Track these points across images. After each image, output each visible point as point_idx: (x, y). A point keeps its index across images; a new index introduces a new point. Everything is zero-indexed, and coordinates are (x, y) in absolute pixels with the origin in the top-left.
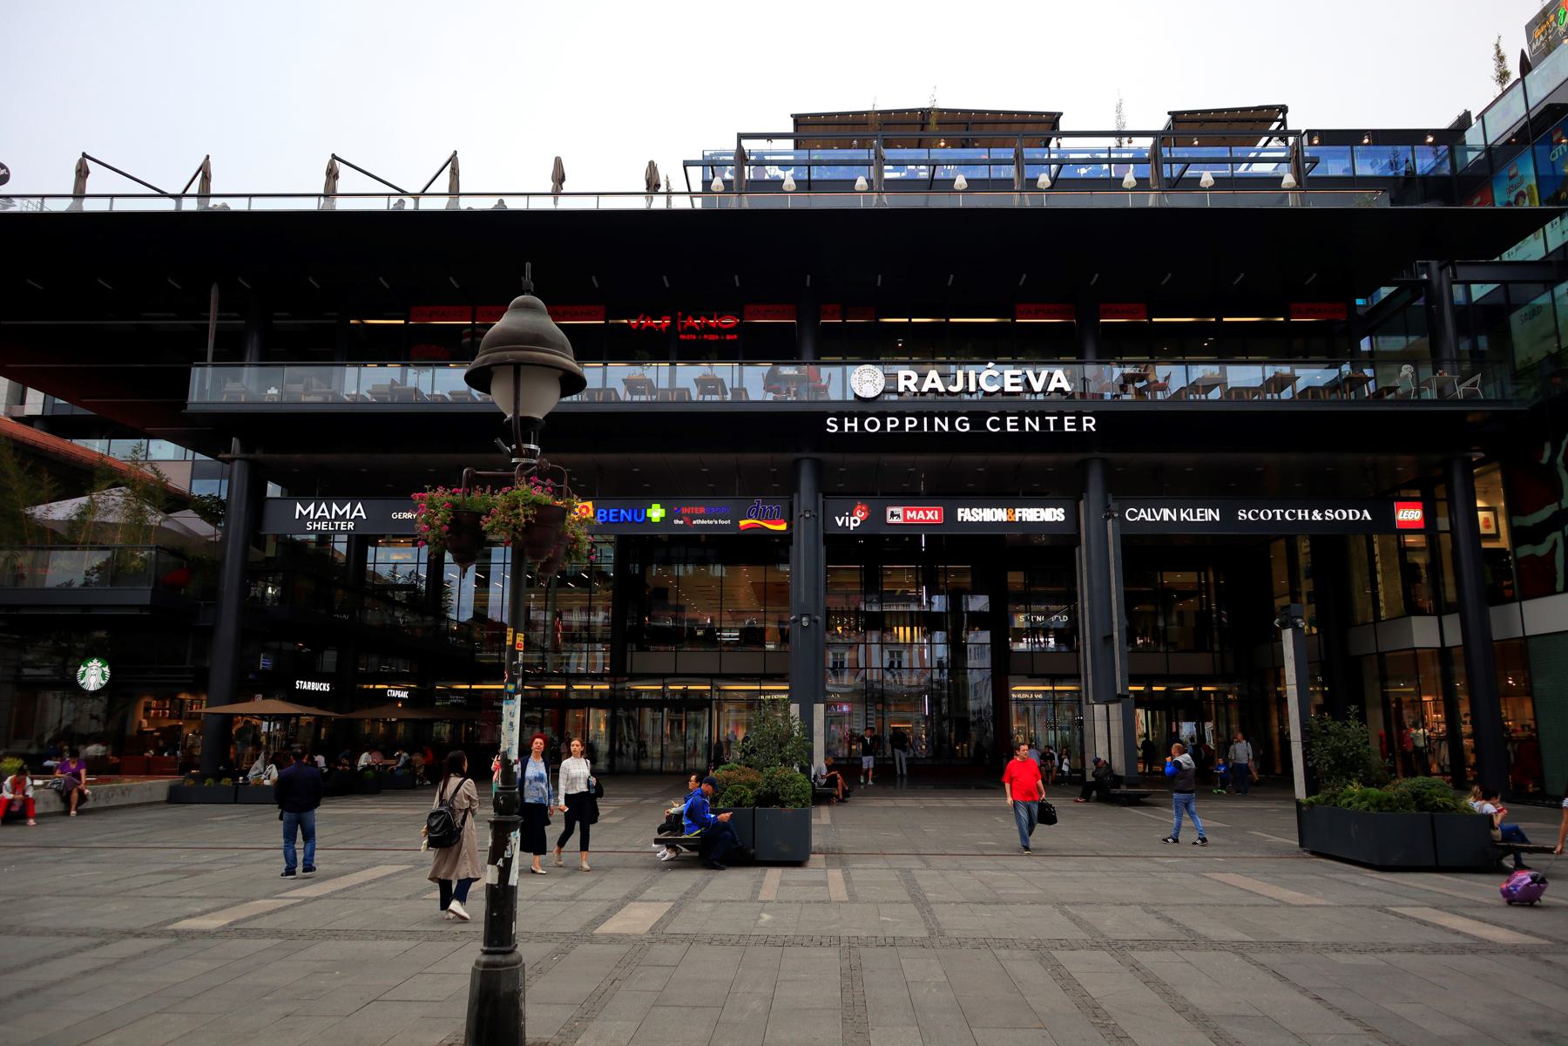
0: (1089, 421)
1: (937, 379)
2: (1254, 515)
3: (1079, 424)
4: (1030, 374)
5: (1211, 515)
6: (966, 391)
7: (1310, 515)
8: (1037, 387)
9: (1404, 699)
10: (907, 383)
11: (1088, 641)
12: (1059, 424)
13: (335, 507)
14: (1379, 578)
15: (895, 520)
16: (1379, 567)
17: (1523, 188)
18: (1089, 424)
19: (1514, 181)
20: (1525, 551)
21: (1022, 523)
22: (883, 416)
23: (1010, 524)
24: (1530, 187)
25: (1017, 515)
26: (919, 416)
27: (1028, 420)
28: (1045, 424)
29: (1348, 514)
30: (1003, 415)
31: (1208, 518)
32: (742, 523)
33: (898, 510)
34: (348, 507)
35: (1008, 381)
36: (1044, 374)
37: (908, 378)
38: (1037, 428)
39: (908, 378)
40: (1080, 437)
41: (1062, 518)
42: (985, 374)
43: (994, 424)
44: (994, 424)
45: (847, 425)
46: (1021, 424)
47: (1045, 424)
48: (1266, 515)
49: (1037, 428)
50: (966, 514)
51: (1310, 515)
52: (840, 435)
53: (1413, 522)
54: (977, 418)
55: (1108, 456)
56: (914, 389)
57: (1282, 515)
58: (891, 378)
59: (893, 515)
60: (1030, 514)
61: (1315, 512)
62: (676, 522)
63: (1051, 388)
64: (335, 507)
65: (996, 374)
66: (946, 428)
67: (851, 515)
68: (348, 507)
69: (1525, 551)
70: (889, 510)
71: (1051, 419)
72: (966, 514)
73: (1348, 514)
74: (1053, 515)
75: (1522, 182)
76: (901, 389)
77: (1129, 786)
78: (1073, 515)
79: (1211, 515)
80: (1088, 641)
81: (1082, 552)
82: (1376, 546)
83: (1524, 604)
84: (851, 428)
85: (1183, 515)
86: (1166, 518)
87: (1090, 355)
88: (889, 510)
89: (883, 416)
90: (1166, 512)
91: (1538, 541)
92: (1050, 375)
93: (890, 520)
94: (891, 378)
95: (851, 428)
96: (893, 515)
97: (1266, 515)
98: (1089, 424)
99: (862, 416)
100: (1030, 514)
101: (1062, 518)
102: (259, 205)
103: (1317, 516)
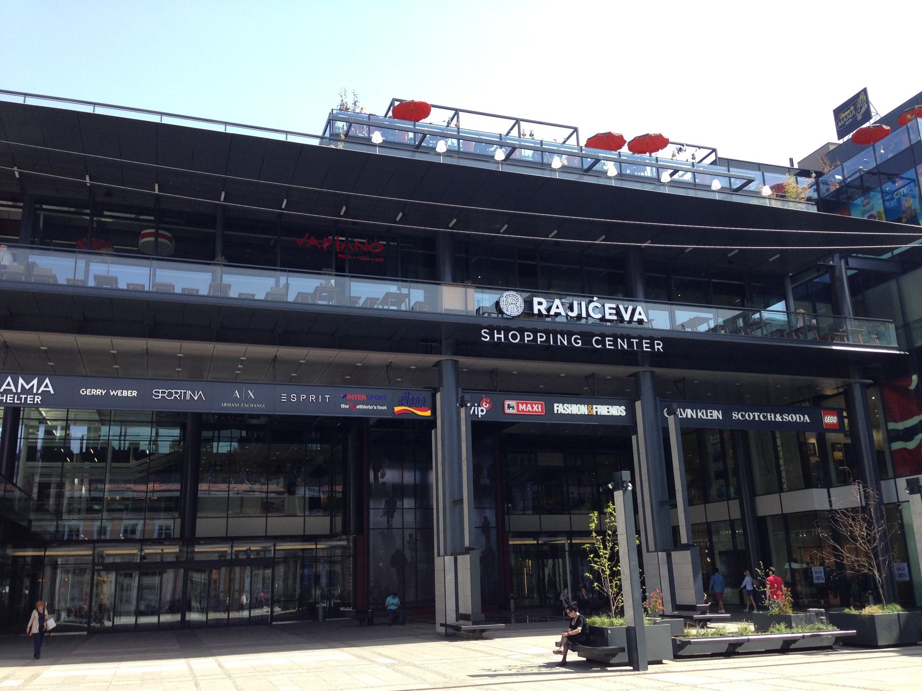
0: (659, 344)
1: (560, 306)
2: (743, 416)
3: (652, 346)
4: (621, 307)
5: (716, 415)
6: (579, 317)
7: (775, 417)
8: (627, 317)
9: (60, 561)
10: (540, 307)
11: (441, 505)
12: (640, 345)
13: (21, 381)
14: (781, 462)
15: (511, 411)
16: (781, 454)
17: (874, 213)
18: (659, 347)
19: (867, 208)
20: (897, 445)
21: (597, 416)
22: (522, 331)
23: (589, 416)
24: (879, 213)
25: (595, 410)
26: (547, 332)
27: (619, 340)
28: (630, 344)
29: (796, 418)
30: (603, 336)
31: (715, 417)
32: (397, 409)
33: (513, 403)
34: (35, 382)
35: (607, 311)
36: (630, 309)
37: (540, 303)
38: (626, 347)
39: (540, 303)
40: (654, 355)
41: (624, 414)
42: (592, 305)
43: (597, 342)
44: (597, 342)
45: (496, 336)
46: (615, 343)
47: (630, 344)
48: (749, 416)
49: (626, 347)
50: (560, 408)
51: (775, 417)
52: (491, 343)
53: (833, 424)
54: (586, 336)
55: (657, 370)
56: (544, 312)
57: (759, 416)
58: (529, 304)
59: (509, 407)
60: (602, 410)
61: (778, 415)
62: (343, 406)
63: (635, 319)
64: (21, 381)
65: (599, 306)
66: (566, 343)
67: (479, 406)
68: (35, 382)
69: (897, 445)
70: (507, 402)
71: (635, 341)
72: (560, 408)
73: (796, 418)
74: (618, 411)
75: (872, 209)
76: (536, 311)
77: (474, 623)
78: (631, 411)
79: (716, 415)
80: (441, 505)
81: (437, 435)
82: (778, 441)
83: (897, 480)
84: (499, 339)
85: (700, 414)
86: (689, 416)
87: (641, 295)
88: (507, 402)
89: (522, 331)
90: (689, 411)
91: (910, 438)
92: (634, 311)
93: (507, 411)
94: (529, 304)
95: (499, 339)
96: (509, 407)
97: (749, 416)
98: (659, 347)
99: (507, 330)
100: (602, 410)
101: (624, 414)
102: (292, 139)
103: (779, 418)
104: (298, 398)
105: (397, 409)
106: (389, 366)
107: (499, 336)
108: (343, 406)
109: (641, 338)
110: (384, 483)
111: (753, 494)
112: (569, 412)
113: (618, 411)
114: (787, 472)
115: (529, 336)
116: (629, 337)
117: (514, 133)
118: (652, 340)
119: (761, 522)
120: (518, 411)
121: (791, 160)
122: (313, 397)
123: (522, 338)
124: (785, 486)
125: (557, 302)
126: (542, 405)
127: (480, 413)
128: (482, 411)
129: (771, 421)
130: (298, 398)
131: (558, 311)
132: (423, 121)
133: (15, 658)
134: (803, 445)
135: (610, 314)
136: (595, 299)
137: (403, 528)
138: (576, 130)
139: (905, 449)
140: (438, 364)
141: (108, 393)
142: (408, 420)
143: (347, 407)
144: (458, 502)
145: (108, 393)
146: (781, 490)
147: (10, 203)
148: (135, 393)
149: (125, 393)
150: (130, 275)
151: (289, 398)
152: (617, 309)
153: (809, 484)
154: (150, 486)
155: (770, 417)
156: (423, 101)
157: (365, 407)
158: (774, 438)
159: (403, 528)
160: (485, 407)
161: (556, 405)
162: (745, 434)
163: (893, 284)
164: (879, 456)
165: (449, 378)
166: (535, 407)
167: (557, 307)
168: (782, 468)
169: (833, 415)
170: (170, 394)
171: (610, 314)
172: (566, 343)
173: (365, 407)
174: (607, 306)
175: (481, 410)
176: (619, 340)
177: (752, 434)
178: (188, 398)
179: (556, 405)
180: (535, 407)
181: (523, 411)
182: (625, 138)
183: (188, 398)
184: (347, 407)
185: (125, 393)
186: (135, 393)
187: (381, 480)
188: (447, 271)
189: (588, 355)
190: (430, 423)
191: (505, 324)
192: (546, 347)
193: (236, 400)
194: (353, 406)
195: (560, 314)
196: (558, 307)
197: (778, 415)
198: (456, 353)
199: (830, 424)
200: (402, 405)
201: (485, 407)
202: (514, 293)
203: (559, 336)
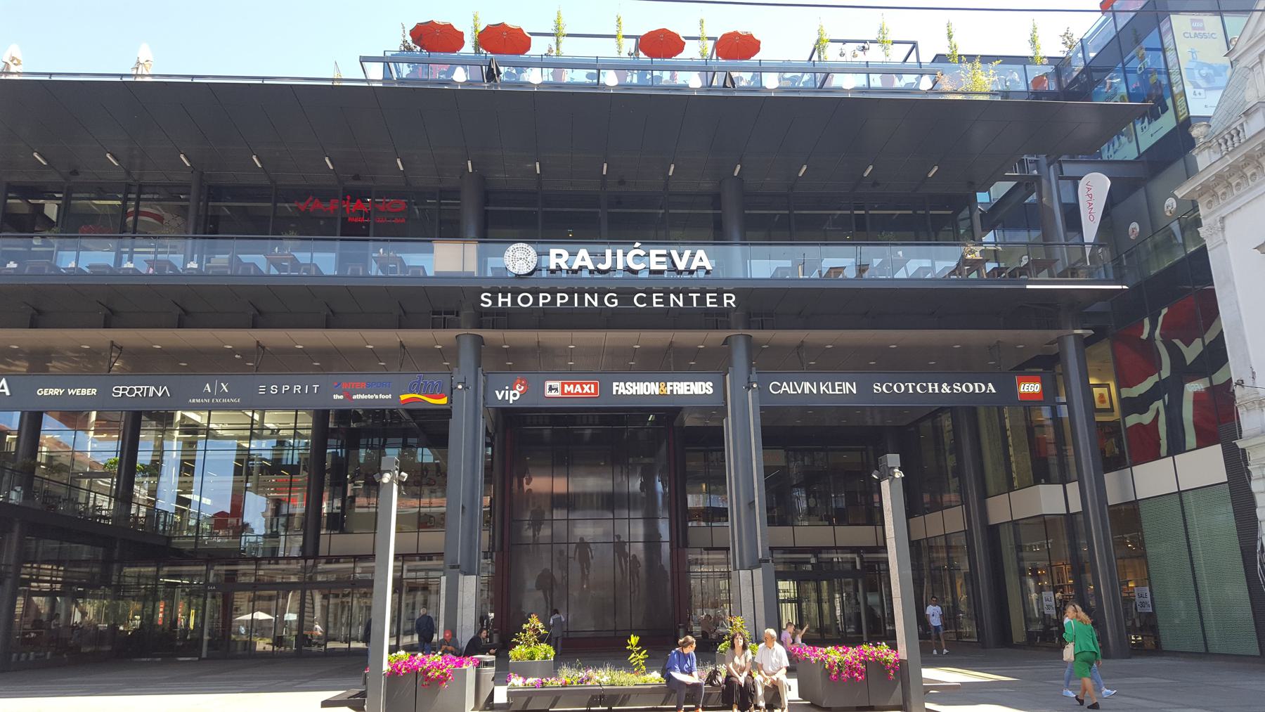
1: (705, 258)
4: (674, 254)
5: (848, 388)
7: (940, 388)
12: (701, 300)
14: (1011, 452)
15: (553, 394)
18: (729, 301)
25: (669, 388)
26: (571, 293)
27: (672, 296)
28: (688, 301)
30: (649, 292)
31: (846, 391)
33: (557, 384)
36: (687, 253)
37: (559, 255)
38: (681, 304)
39: (559, 255)
42: (632, 253)
43: (641, 300)
45: (500, 300)
47: (688, 301)
49: (681, 304)
50: (622, 388)
51: (940, 388)
53: (1034, 394)
54: (625, 294)
57: (914, 388)
59: (551, 389)
61: (945, 385)
62: (336, 397)
66: (595, 304)
69: (1132, 420)
70: (548, 384)
71: (695, 295)
72: (622, 388)
74: (701, 388)
78: (720, 388)
79: (848, 388)
84: (504, 303)
88: (548, 384)
92: (693, 255)
93: (548, 394)
95: (504, 303)
96: (551, 389)
98: (729, 301)
103: (946, 388)
104: (280, 389)
105: (403, 397)
106: (801, 346)
108: (336, 397)
109: (703, 292)
110: (530, 490)
111: (984, 495)
113: (701, 388)
114: (1017, 463)
115: (562, 298)
116: (686, 292)
117: (913, 58)
118: (720, 292)
119: (993, 532)
121: (476, 19)
122: (297, 388)
124: (1016, 484)
126: (596, 385)
127: (512, 398)
128: (515, 395)
129: (934, 393)
130: (280, 389)
133: (313, 678)
134: (1032, 429)
136: (637, 245)
138: (915, 45)
139: (1139, 425)
140: (727, 341)
141: (66, 392)
142: (425, 410)
144: (752, 504)
145: (66, 392)
146: (1011, 488)
147: (87, 195)
148: (94, 391)
149: (84, 392)
150: (139, 259)
152: (669, 255)
156: (731, 31)
157: (364, 397)
158: (1002, 418)
159: (552, 544)
160: (519, 389)
161: (615, 384)
162: (973, 412)
163: (1141, 192)
165: (467, 356)
168: (1012, 459)
169: (1035, 381)
170: (131, 391)
172: (595, 304)
173: (364, 397)
176: (672, 296)
177: (982, 413)
178: (151, 394)
179: (615, 384)
181: (569, 393)
182: (458, 27)
183: (151, 394)
185: (84, 392)
188: (471, 225)
189: (670, 319)
190: (445, 413)
191: (516, 285)
192: (568, 310)
193: (207, 395)
194: (348, 396)
196: (583, 258)
197: (945, 385)
198: (749, 326)
200: (411, 392)
201: (519, 389)
202: (525, 245)
203: (587, 296)
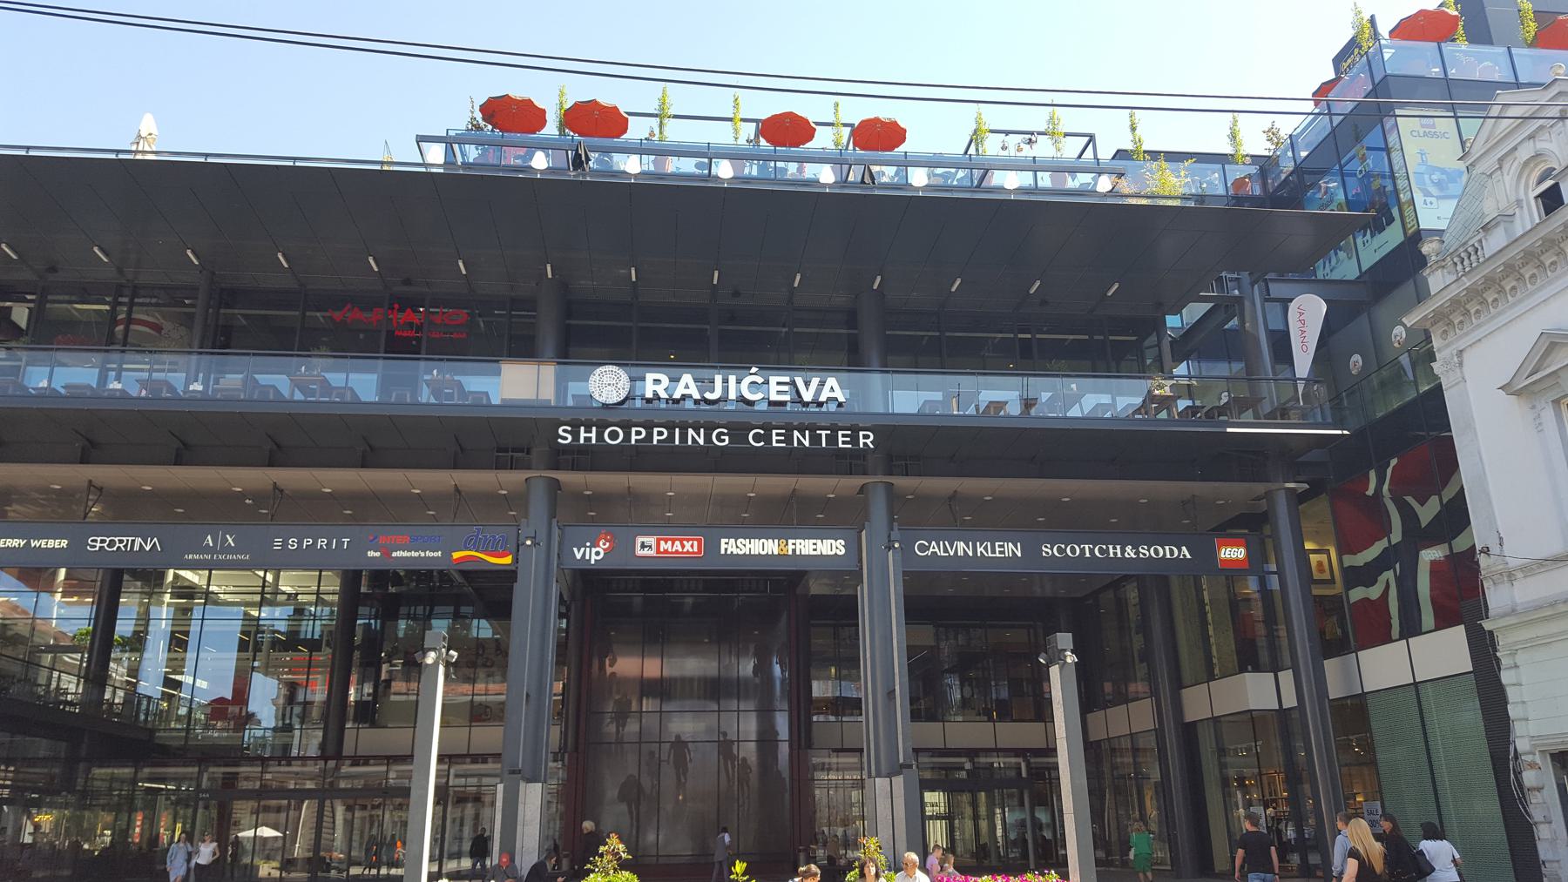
0: (866, 437)
2: (1060, 550)
3: (854, 440)
4: (799, 381)
5: (1011, 549)
7: (1123, 551)
12: (832, 439)
15: (646, 552)
18: (866, 440)
20: (1357, 594)
25: (791, 547)
27: (796, 433)
28: (815, 439)
30: (768, 428)
32: (456, 555)
33: (651, 540)
37: (657, 381)
38: (807, 443)
39: (657, 381)
43: (757, 438)
47: (815, 439)
49: (807, 443)
50: (732, 546)
51: (1123, 551)
53: (1237, 561)
54: (738, 431)
56: (663, 395)
59: (643, 546)
60: (806, 547)
61: (1128, 549)
62: (371, 554)
69: (1357, 594)
70: (640, 540)
71: (824, 433)
72: (732, 546)
74: (831, 547)
78: (854, 547)
79: (1011, 549)
84: (588, 439)
88: (640, 540)
93: (640, 552)
95: (588, 439)
96: (643, 546)
98: (866, 440)
103: (1130, 552)
104: (300, 543)
105: (456, 555)
107: (588, 436)
108: (371, 554)
109: (834, 429)
111: (1178, 684)
112: (745, 551)
113: (831, 547)
115: (660, 434)
116: (813, 429)
117: (1089, 154)
118: (855, 430)
119: (1189, 732)
120: (658, 551)
122: (322, 543)
123: (627, 437)
124: (1217, 671)
125: (832, 381)
126: (699, 541)
127: (594, 557)
128: (597, 553)
130: (300, 543)
131: (687, 392)
132: (808, 145)
135: (779, 392)
136: (754, 370)
137: (640, 743)
143: (378, 554)
145: (28, 543)
146: (1211, 677)
148: (64, 543)
151: (285, 543)
152: (793, 383)
153: (1248, 660)
154: (480, 687)
155: (1114, 551)
156: (872, 116)
157: (406, 554)
159: (640, 743)
160: (603, 546)
161: (723, 541)
163: (1363, 321)
164: (1325, 607)
166: (688, 546)
167: (687, 387)
168: (1212, 640)
169: (1238, 545)
170: (111, 544)
171: (779, 392)
173: (406, 554)
174: (773, 380)
175: (593, 554)
176: (796, 433)
178: (136, 548)
179: (723, 541)
180: (688, 546)
181: (666, 551)
183: (136, 548)
184: (378, 554)
186: (64, 543)
187: (609, 670)
191: (603, 416)
192: (666, 447)
195: (690, 396)
197: (1128, 549)
199: (1231, 561)
201: (603, 546)
202: (615, 368)
